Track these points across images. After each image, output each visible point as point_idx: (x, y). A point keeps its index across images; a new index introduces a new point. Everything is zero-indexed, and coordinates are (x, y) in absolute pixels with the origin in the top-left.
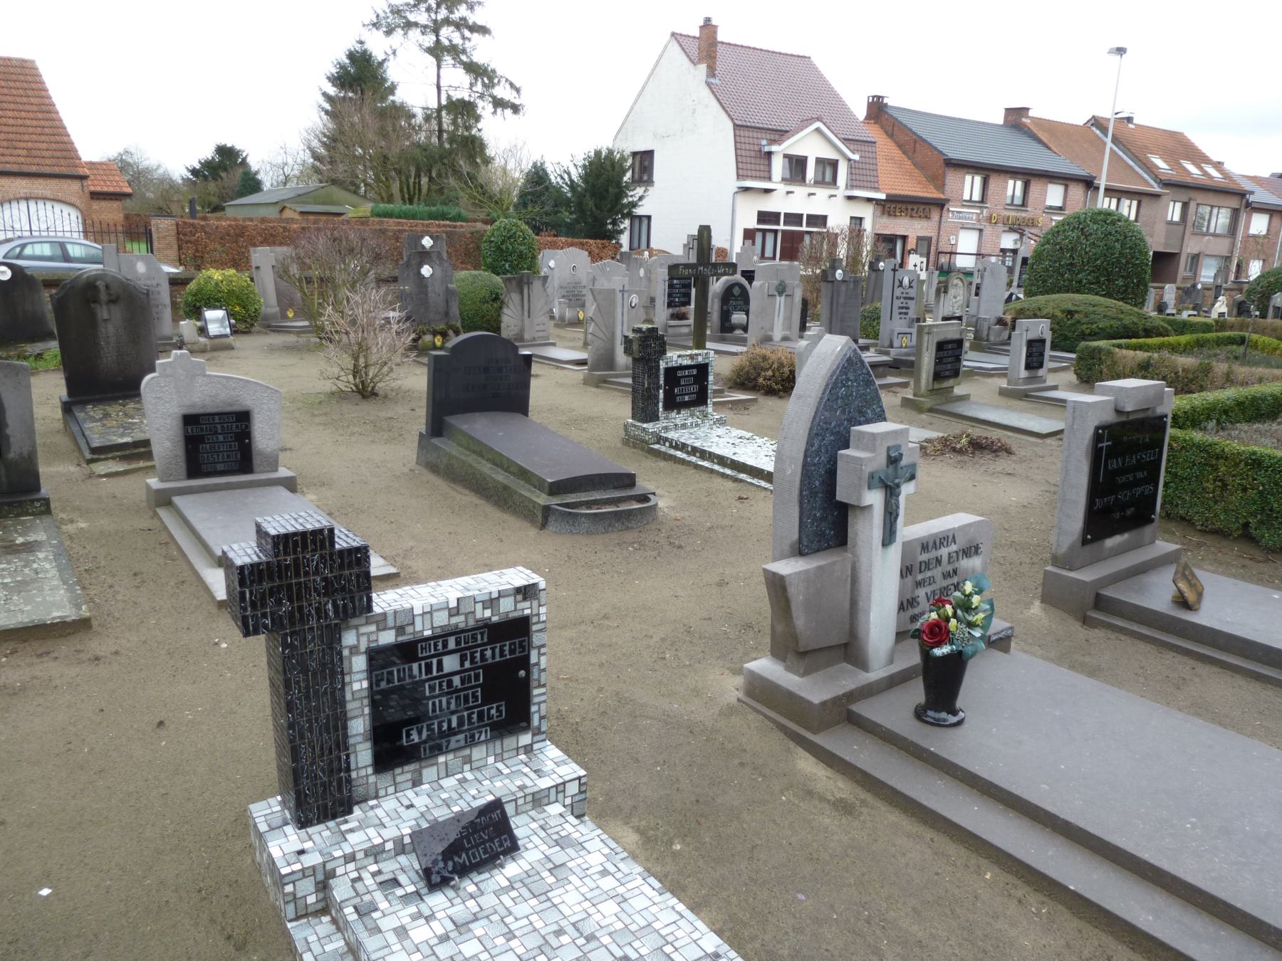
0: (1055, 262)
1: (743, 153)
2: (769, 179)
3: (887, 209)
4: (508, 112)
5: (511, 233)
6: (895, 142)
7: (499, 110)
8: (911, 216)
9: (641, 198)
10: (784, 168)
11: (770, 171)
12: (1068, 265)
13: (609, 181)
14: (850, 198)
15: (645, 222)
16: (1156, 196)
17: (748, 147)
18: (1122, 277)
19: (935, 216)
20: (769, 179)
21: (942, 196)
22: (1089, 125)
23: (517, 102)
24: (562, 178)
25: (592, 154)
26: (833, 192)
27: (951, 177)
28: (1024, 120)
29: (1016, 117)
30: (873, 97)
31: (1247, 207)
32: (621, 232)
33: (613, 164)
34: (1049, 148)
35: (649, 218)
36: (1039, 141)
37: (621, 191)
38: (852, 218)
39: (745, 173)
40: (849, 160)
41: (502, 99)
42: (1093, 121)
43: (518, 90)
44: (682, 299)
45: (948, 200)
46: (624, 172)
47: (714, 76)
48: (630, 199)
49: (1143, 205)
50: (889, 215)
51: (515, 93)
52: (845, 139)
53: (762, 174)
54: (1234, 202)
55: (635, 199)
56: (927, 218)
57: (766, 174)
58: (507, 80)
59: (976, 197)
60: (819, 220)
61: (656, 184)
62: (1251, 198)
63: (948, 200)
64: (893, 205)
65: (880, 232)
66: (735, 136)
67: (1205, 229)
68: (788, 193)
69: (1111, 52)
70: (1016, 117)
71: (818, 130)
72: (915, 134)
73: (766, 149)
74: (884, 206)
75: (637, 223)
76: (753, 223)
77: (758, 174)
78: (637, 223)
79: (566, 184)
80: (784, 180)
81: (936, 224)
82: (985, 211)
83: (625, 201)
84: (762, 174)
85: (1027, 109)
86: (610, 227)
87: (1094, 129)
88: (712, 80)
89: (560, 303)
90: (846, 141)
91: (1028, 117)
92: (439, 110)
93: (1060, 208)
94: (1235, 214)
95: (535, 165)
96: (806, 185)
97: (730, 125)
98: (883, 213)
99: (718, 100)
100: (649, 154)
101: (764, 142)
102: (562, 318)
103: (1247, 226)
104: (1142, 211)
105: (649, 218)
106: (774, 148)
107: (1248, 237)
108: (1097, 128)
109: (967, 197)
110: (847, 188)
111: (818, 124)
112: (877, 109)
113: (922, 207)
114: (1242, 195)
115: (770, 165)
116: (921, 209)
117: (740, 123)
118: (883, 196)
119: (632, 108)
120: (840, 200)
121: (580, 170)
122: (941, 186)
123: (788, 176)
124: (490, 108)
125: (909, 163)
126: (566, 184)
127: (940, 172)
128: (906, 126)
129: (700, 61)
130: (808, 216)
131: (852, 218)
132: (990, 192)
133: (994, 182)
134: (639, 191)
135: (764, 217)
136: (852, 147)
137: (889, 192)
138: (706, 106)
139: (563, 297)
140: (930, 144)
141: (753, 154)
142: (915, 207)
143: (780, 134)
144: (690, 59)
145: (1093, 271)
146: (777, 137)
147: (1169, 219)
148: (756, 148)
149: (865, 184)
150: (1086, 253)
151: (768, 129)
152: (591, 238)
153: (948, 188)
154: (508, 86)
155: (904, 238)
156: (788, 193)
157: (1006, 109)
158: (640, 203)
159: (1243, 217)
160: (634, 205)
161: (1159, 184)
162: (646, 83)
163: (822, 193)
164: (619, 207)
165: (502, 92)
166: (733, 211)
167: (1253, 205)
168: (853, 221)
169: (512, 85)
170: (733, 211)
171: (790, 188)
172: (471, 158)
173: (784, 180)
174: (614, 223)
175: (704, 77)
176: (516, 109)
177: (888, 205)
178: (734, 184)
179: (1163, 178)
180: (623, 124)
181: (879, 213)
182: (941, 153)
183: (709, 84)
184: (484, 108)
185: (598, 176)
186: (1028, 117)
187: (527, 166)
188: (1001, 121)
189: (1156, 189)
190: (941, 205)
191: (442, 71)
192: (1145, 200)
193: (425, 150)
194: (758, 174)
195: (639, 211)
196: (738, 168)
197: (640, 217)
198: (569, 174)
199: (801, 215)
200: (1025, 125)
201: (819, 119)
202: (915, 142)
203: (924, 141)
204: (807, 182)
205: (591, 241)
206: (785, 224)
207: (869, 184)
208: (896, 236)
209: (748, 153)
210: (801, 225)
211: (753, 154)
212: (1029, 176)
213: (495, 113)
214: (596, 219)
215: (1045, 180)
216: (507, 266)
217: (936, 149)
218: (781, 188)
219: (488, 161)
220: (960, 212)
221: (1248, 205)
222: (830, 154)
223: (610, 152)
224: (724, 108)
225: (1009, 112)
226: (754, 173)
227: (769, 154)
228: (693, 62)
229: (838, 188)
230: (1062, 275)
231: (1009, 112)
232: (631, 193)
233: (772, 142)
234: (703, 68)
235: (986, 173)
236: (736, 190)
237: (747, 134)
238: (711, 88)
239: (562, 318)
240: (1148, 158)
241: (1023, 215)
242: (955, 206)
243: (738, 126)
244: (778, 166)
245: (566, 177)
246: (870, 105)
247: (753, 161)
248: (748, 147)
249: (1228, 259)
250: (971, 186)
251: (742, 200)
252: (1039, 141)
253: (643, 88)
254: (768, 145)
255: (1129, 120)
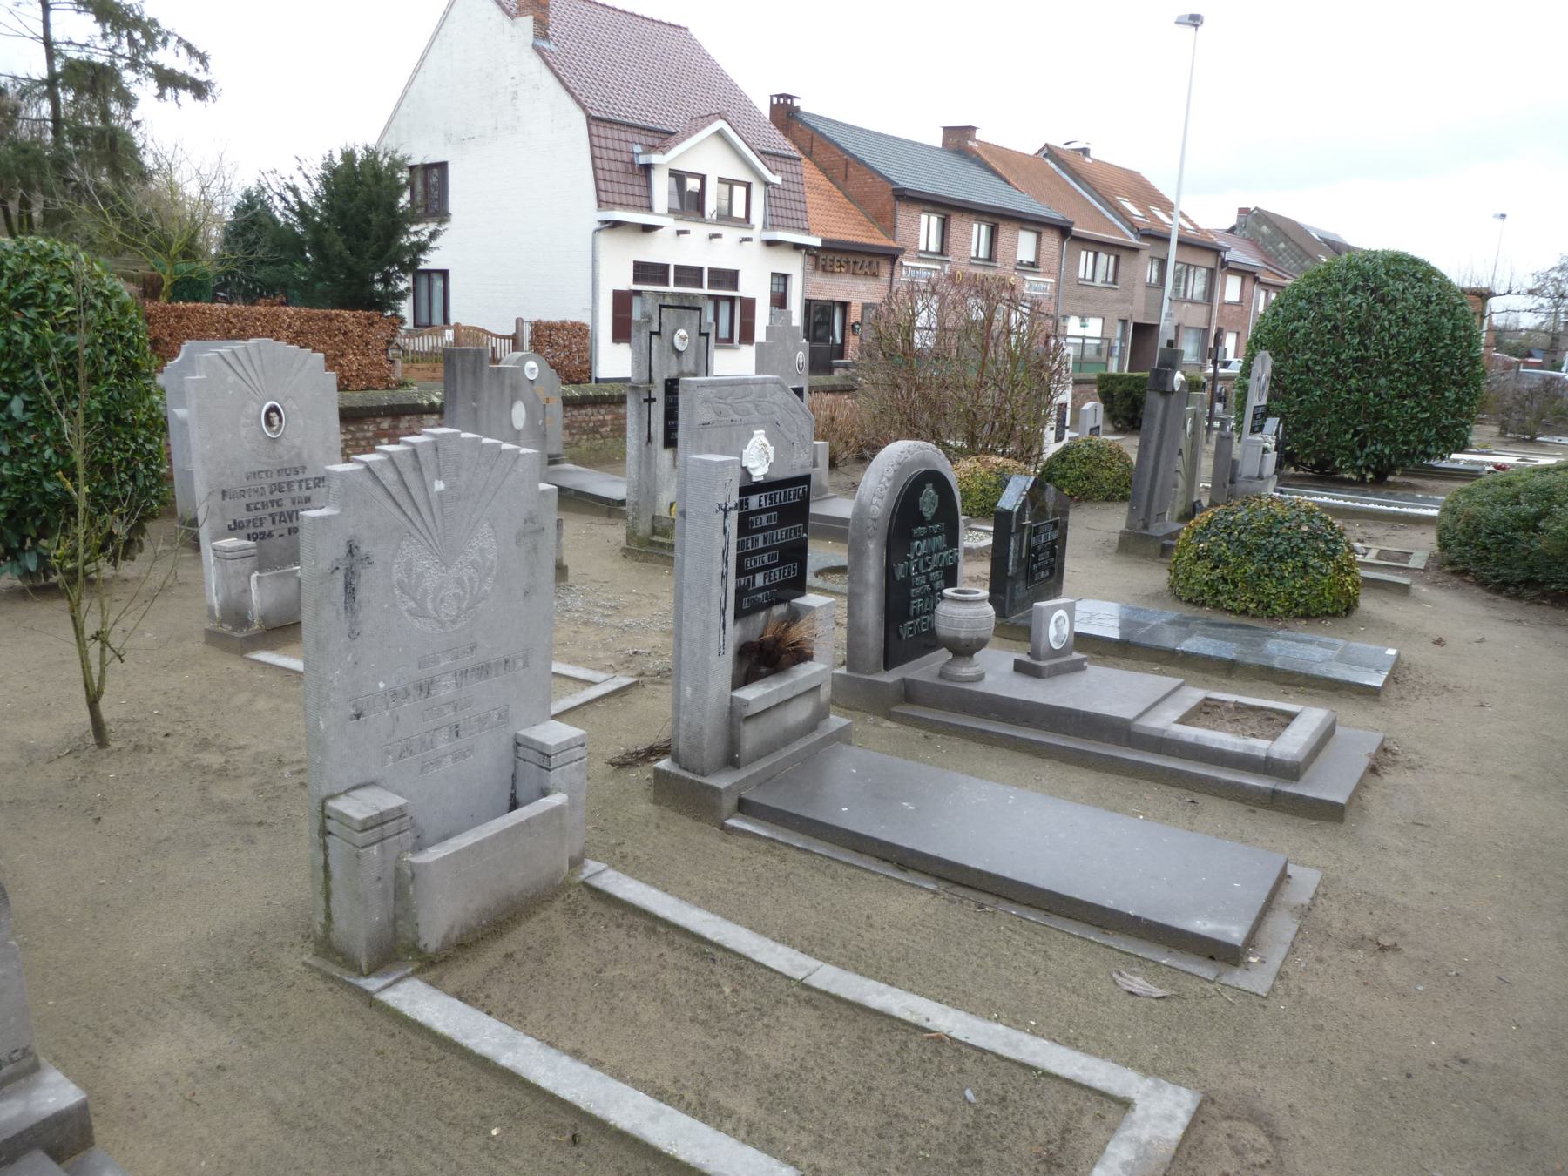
0: (1324, 354)
1: (606, 164)
2: (650, 209)
3: (821, 262)
4: (186, 96)
5: (24, 287)
6: (816, 164)
7: (169, 92)
8: (854, 274)
9: (433, 235)
10: (670, 193)
11: (649, 197)
12: (1356, 360)
13: (372, 205)
14: (770, 243)
15: (438, 284)
16: (1134, 250)
17: (612, 155)
18: (1455, 383)
19: (885, 271)
20: (650, 209)
21: (892, 244)
22: (1042, 155)
23: (201, 77)
24: (283, 199)
25: (338, 161)
26: (745, 233)
27: (903, 215)
28: (970, 143)
29: (958, 139)
30: (779, 96)
31: (1222, 267)
32: (401, 296)
33: (378, 176)
34: (1008, 183)
35: (444, 274)
36: (995, 173)
37: (396, 224)
38: (773, 274)
39: (610, 198)
40: (767, 184)
41: (172, 71)
42: (1046, 151)
43: (203, 59)
44: (778, 574)
45: (902, 251)
46: (399, 190)
47: (546, 37)
48: (414, 239)
49: (1122, 261)
50: (824, 270)
51: (196, 63)
52: (763, 153)
53: (638, 201)
54: (1209, 261)
55: (423, 239)
56: (875, 275)
57: (644, 202)
58: (180, 40)
59: (934, 246)
60: (727, 278)
61: (454, 218)
62: (1228, 256)
63: (902, 251)
64: (829, 256)
65: (812, 297)
66: (590, 135)
67: (1182, 296)
68: (679, 233)
69: (1495, 216)
70: (958, 139)
71: (720, 134)
72: (846, 152)
73: (642, 160)
74: (817, 257)
75: (424, 281)
76: (626, 283)
77: (631, 200)
78: (424, 281)
79: (292, 210)
80: (671, 211)
81: (886, 284)
82: (947, 266)
83: (404, 241)
84: (638, 201)
85: (973, 129)
86: (379, 287)
87: (1048, 161)
88: (544, 44)
89: (221, 555)
90: (762, 154)
91: (974, 140)
92: (52, 81)
93: (1032, 265)
94: (1212, 273)
95: (248, 196)
96: (705, 222)
97: (580, 118)
98: (816, 268)
99: (557, 76)
100: (442, 166)
101: (638, 149)
102: (236, 615)
103: (1223, 293)
104: (1121, 268)
105: (444, 274)
106: (655, 158)
107: (1225, 304)
108: (1052, 160)
109: (922, 247)
110: (765, 228)
111: (720, 124)
112: (785, 113)
113: (867, 260)
114: (1216, 251)
115: (649, 186)
116: (867, 263)
117: (597, 114)
118: (817, 242)
119: (405, 93)
120: (755, 247)
121: (316, 185)
122: (890, 230)
123: (677, 206)
124: (152, 86)
125: (840, 194)
126: (292, 210)
127: (888, 208)
128: (830, 140)
129: (521, 11)
130: (711, 271)
131: (773, 274)
132: (951, 240)
133: (957, 224)
134: (424, 229)
135: (643, 271)
136: (773, 165)
137: (830, 236)
138: (537, 87)
139: (235, 528)
140: (870, 167)
141: (621, 167)
142: (859, 260)
143: (664, 138)
144: (504, 9)
145: (1408, 374)
146: (657, 142)
147: (922, 247)
148: (626, 157)
149: (790, 222)
150: (1392, 337)
151: (643, 128)
152: (343, 306)
153: (899, 232)
154: (183, 51)
155: (845, 306)
156: (679, 233)
157: (945, 128)
158: (433, 244)
159: (1219, 278)
160: (422, 248)
161: (1136, 234)
162: (428, 49)
163: (731, 234)
164: (393, 250)
165: (167, 57)
166: (594, 261)
167: (1231, 265)
168: (776, 281)
169: (190, 49)
170: (594, 261)
171: (683, 226)
172: (116, 172)
173: (671, 211)
174: (386, 280)
175: (530, 39)
176: (200, 90)
177: (822, 257)
178: (593, 216)
179: (1141, 227)
180: (391, 120)
181: (810, 268)
182: (887, 179)
183: (539, 51)
184: (143, 89)
185: (351, 195)
186: (974, 140)
187: (237, 197)
188: (939, 145)
189: (1133, 240)
190: (892, 256)
191: (53, 16)
192: (1124, 255)
193: (25, 151)
194: (631, 200)
195: (431, 261)
196: (598, 190)
197: (429, 272)
198: (295, 190)
199: (701, 269)
200: (972, 150)
201: (721, 116)
202: (847, 163)
203: (861, 162)
204: (707, 216)
205: (346, 313)
206: (678, 282)
207: (795, 223)
208: (833, 302)
209: (613, 166)
210: (666, 283)
211: (621, 167)
212: (997, 218)
213: (161, 96)
214: (351, 273)
215: (1017, 225)
216: (16, 406)
217: (880, 174)
218: (671, 224)
219: (144, 176)
220: (918, 268)
221: (1224, 264)
222: (739, 173)
223: (372, 154)
224: (567, 89)
225: (949, 131)
226: (624, 199)
227: (647, 168)
228: (508, 13)
229: (752, 228)
230: (1345, 380)
231: (949, 131)
232: (414, 228)
233: (651, 149)
234: (527, 22)
235: (946, 212)
236: (598, 226)
237: (609, 133)
238: (543, 57)
239: (236, 615)
240: (1117, 201)
241: (992, 273)
242: (910, 259)
243: (594, 118)
244: (662, 186)
245: (290, 196)
246: (774, 109)
247: (622, 178)
248: (612, 155)
249: (1206, 331)
250: (927, 228)
251: (607, 241)
252: (995, 173)
253: (423, 58)
254: (644, 153)
255: (1085, 151)
